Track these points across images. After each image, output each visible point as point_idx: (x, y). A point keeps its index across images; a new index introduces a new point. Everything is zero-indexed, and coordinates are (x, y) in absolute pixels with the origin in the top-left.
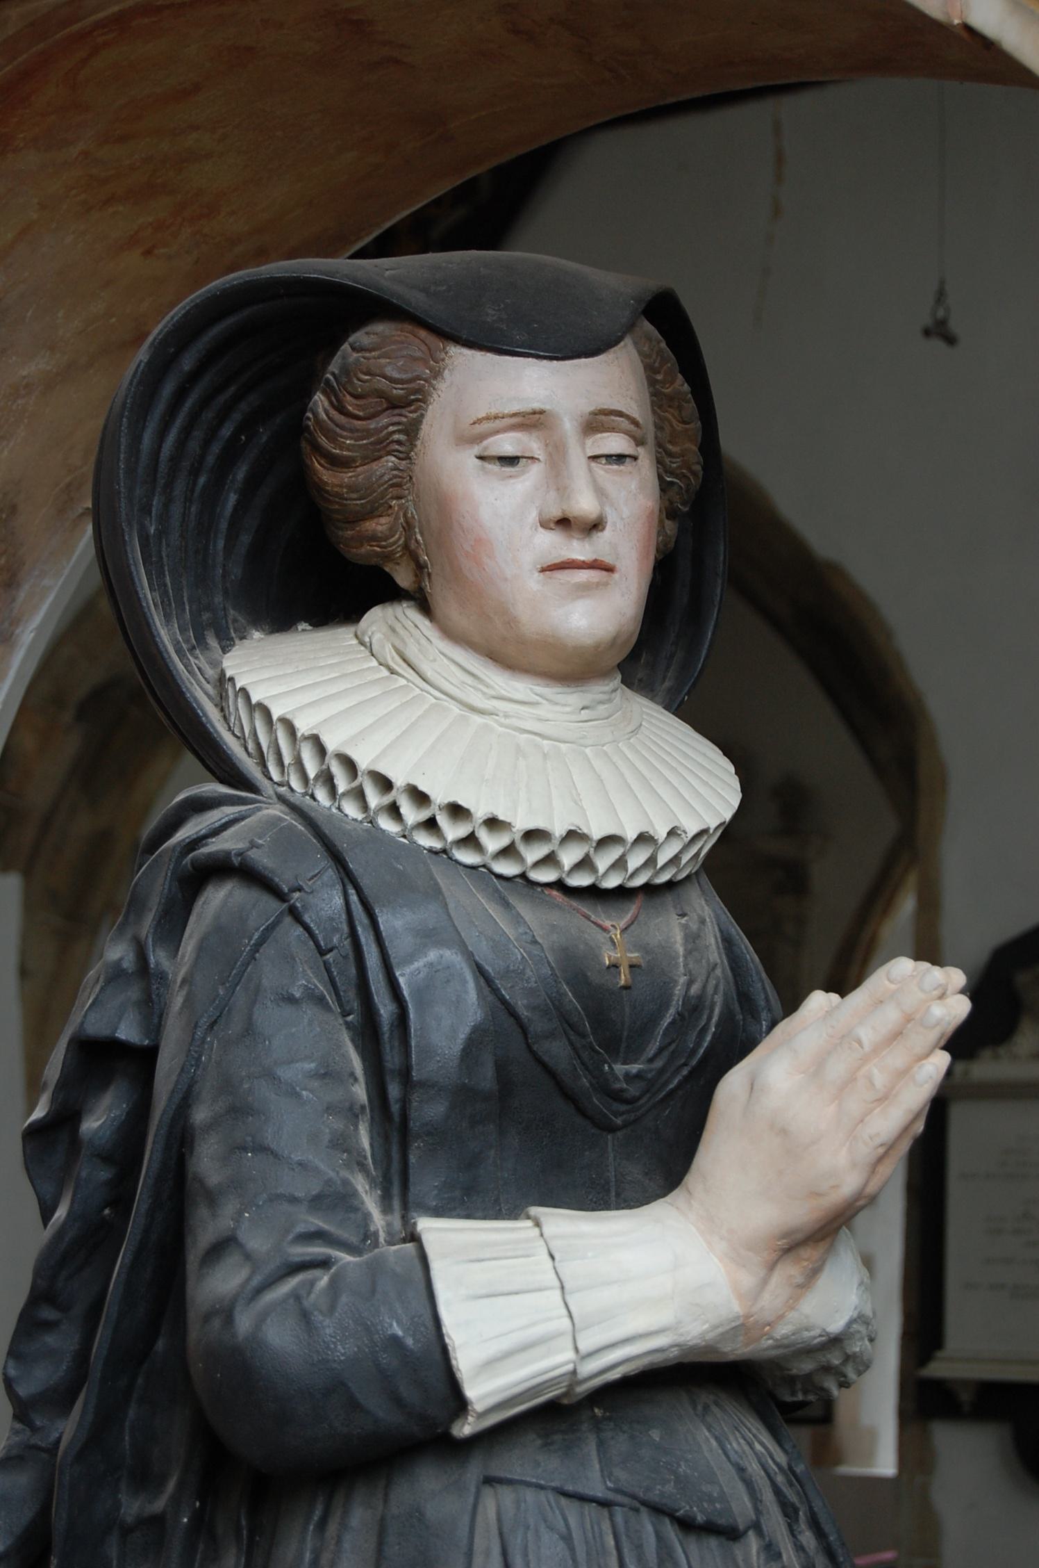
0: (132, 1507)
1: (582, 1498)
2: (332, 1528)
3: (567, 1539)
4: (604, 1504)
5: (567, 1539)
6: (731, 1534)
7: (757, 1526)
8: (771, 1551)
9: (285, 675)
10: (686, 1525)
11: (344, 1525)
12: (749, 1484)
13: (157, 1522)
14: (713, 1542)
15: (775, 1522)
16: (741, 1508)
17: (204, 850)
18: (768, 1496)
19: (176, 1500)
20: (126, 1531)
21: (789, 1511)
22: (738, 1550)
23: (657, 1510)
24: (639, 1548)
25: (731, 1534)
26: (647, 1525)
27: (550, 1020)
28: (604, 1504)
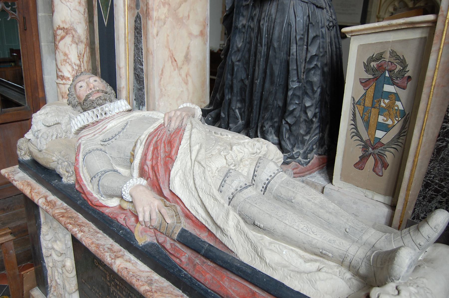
0: (244, 3)
1: (304, 2)
2: (271, 5)
3: (302, 7)
4: (307, 3)
5: (302, 7)
6: (322, 8)
7: (326, 8)
8: (327, 11)
9: (97, 206)
10: (317, 7)
11: (273, 5)
12: (325, 2)
13: (248, 5)
14: (320, 9)
15: (328, 8)
16: (324, 5)
17: (171, 256)
18: (327, 4)
19: (250, 2)
20: (244, 6)
21: (330, 7)
22: (323, 11)
23: (314, 4)
24: (311, 9)
25: (322, 8)
26: (312, 6)
27: (121, 268)
28: (307, 3)
